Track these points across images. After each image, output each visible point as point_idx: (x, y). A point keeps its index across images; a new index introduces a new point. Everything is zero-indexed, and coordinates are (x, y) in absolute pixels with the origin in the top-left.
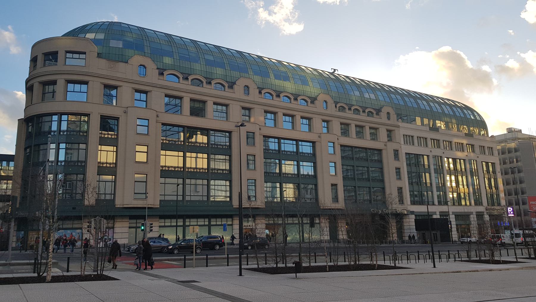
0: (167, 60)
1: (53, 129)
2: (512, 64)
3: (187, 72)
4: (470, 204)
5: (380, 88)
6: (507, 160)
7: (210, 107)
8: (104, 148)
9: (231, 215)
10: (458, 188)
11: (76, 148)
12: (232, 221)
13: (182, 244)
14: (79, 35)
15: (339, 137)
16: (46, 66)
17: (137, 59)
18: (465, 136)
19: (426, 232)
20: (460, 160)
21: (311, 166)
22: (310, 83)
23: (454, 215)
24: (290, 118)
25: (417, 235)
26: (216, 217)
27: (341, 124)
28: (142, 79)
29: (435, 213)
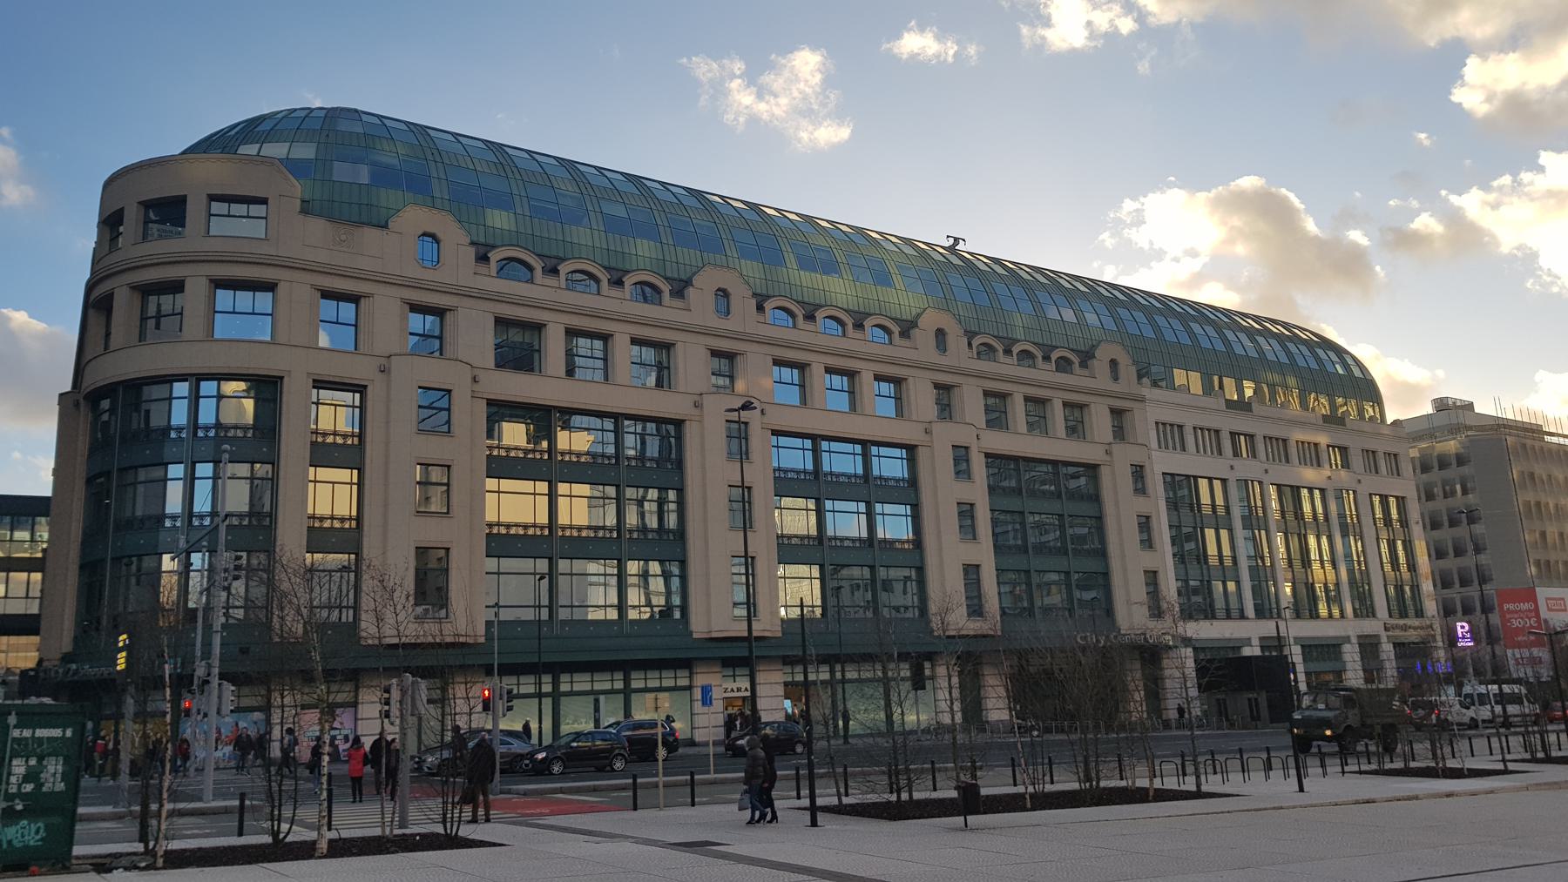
0: (499, 220)
1: (174, 422)
2: (1426, 223)
3: (554, 253)
4: (1342, 616)
5: (1047, 282)
6: (1435, 490)
7: (554, 346)
8: (324, 473)
9: (930, 653)
10: (1309, 570)
11: (245, 475)
12: (691, 678)
13: (572, 747)
14: (241, 147)
15: (980, 432)
16: (150, 238)
17: (414, 218)
18: (1227, 408)
19: (1258, 694)
20: (1311, 490)
21: (906, 516)
22: (897, 280)
23: (1299, 647)
24: (795, 372)
25: (1202, 704)
26: (646, 665)
27: (987, 394)
28: (429, 275)
29: (1248, 642)
